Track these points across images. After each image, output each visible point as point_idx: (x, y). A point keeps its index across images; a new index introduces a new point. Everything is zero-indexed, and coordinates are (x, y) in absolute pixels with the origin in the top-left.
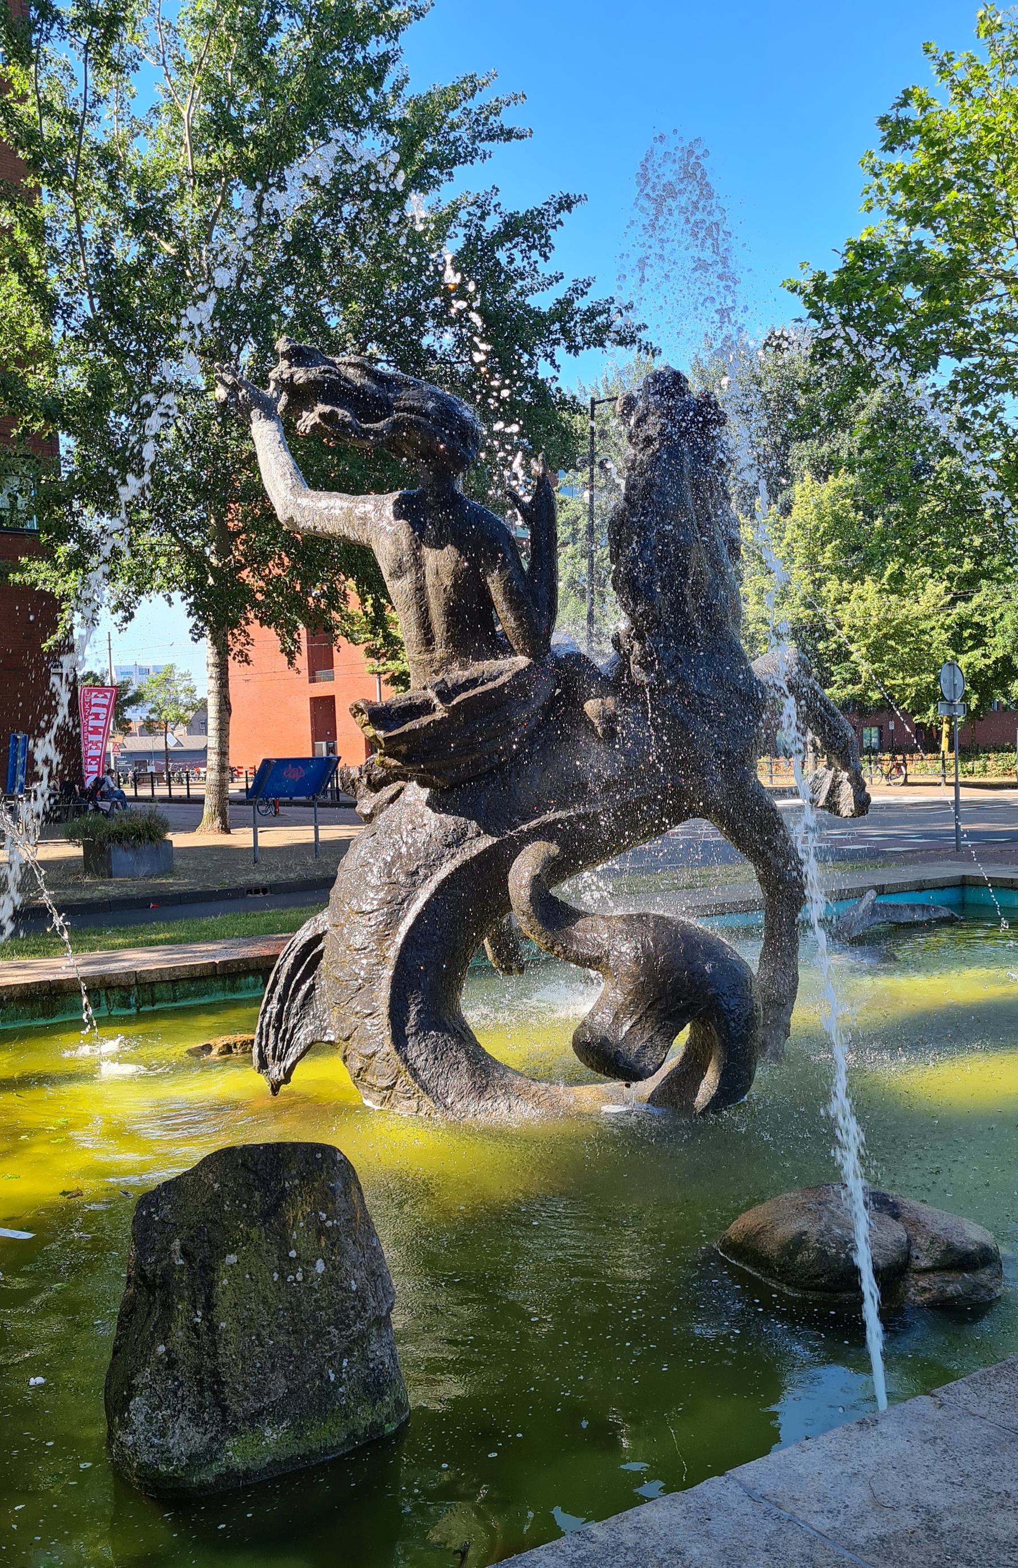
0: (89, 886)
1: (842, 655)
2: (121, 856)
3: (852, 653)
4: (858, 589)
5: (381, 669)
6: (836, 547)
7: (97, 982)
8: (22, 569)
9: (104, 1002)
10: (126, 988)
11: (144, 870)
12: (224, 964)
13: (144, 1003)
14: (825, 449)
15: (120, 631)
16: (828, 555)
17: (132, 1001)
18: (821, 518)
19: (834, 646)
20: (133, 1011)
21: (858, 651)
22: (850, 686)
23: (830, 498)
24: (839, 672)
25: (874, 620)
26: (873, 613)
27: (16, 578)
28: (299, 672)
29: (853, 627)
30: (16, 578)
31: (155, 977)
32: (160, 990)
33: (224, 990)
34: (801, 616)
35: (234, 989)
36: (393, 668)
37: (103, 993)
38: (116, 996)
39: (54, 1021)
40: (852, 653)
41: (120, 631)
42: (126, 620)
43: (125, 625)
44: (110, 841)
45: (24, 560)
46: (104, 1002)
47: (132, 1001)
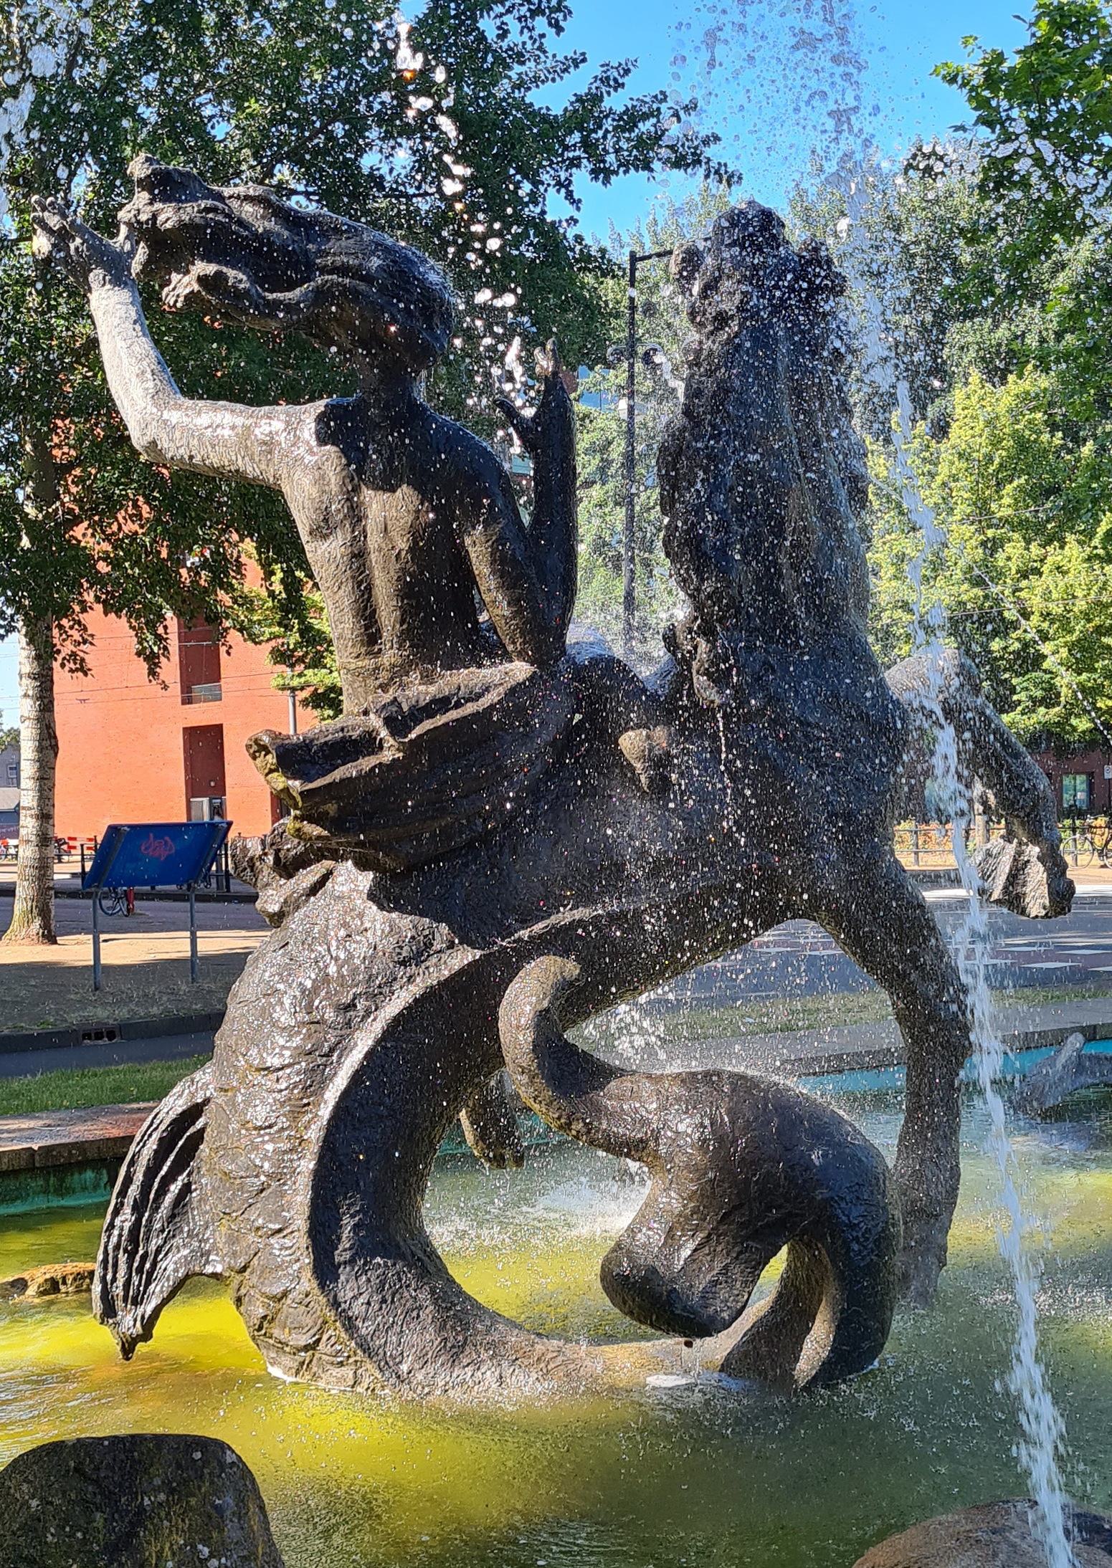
1: (1029, 660)
4: (1054, 556)
12: (47, 1150)
14: (1002, 333)
16: (1007, 501)
18: (996, 442)
19: (1017, 645)
21: (1054, 654)
22: (1042, 710)
25: (1081, 605)
26: (1079, 593)
29: (1046, 616)
33: (46, 1192)
34: (964, 598)
35: (62, 1191)
36: (315, 680)
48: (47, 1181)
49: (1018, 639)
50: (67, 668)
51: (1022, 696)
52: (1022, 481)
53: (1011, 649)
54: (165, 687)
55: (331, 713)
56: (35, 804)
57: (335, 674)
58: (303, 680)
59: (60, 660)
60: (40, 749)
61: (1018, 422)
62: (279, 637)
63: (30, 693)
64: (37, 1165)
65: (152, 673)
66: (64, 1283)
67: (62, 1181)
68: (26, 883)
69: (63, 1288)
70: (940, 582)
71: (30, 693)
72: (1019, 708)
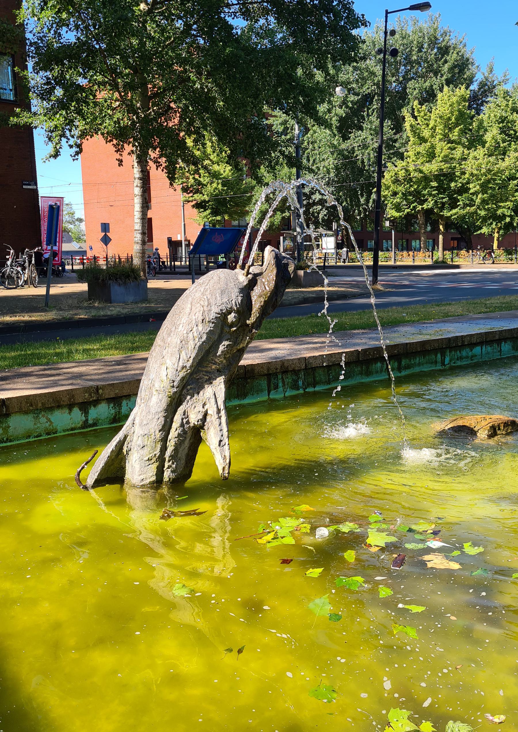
0: (98, 308)
1: (463, 190)
2: (116, 290)
3: (470, 189)
4: (473, 153)
5: (191, 199)
6: (460, 130)
7: (279, 367)
8: (18, 115)
9: (280, 384)
10: (295, 372)
11: (131, 298)
12: (365, 351)
13: (309, 385)
14: (427, 84)
15: (74, 160)
16: (456, 134)
17: (300, 383)
18: (452, 113)
19: (460, 185)
20: (301, 391)
21: (474, 187)
22: (468, 208)
23: (457, 101)
24: (462, 200)
25: (483, 171)
26: (483, 166)
27: (13, 120)
28: (175, 190)
29: (472, 174)
30: (13, 120)
31: (317, 363)
32: (320, 375)
33: (361, 374)
34: (443, 167)
35: (368, 373)
36: (198, 198)
37: (280, 376)
38: (289, 380)
39: (246, 401)
40: (470, 189)
41: (74, 160)
42: (77, 153)
43: (76, 157)
44: (110, 279)
45: (18, 110)
46: (280, 384)
47: (300, 383)
48: (362, 368)
49: (461, 183)
50: (164, 172)
51: (461, 203)
52: (462, 126)
53: (458, 186)
54: (175, 190)
55: (203, 210)
56: (140, 228)
57: (205, 196)
58: (193, 198)
59: (162, 168)
60: (142, 207)
61: (459, 105)
62: (185, 183)
63: (139, 185)
64: (360, 359)
65: (171, 184)
66: (499, 429)
67: (368, 368)
68: (137, 259)
69: (499, 432)
70: (434, 161)
71: (139, 185)
72: (459, 207)
